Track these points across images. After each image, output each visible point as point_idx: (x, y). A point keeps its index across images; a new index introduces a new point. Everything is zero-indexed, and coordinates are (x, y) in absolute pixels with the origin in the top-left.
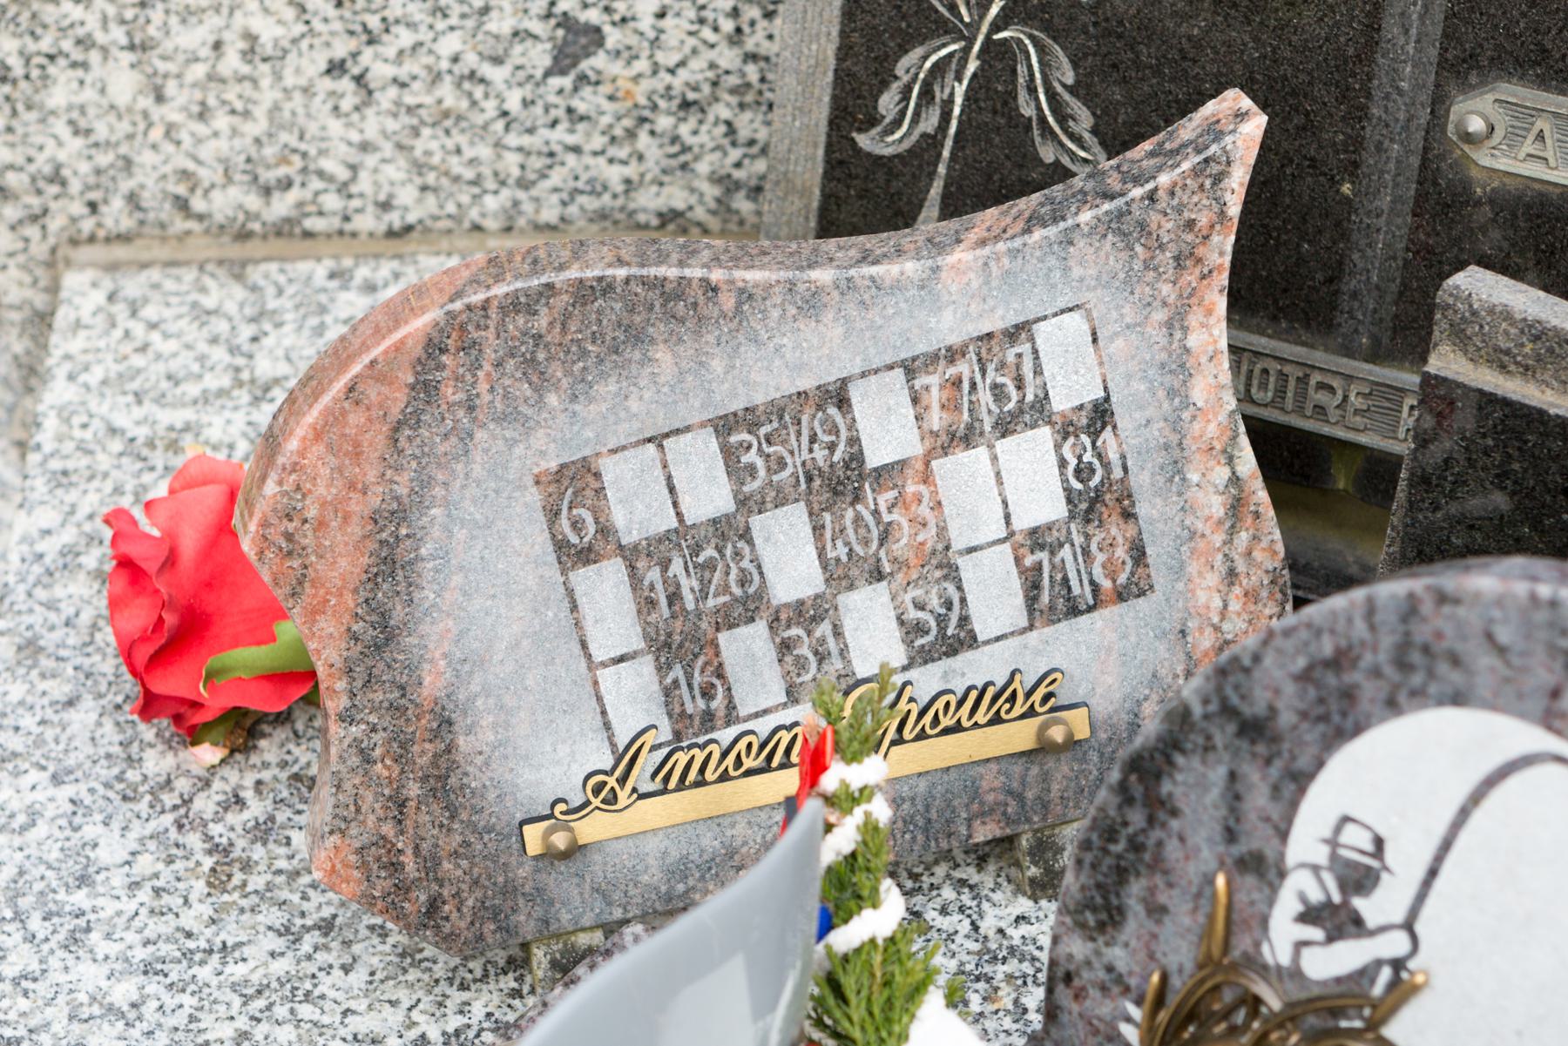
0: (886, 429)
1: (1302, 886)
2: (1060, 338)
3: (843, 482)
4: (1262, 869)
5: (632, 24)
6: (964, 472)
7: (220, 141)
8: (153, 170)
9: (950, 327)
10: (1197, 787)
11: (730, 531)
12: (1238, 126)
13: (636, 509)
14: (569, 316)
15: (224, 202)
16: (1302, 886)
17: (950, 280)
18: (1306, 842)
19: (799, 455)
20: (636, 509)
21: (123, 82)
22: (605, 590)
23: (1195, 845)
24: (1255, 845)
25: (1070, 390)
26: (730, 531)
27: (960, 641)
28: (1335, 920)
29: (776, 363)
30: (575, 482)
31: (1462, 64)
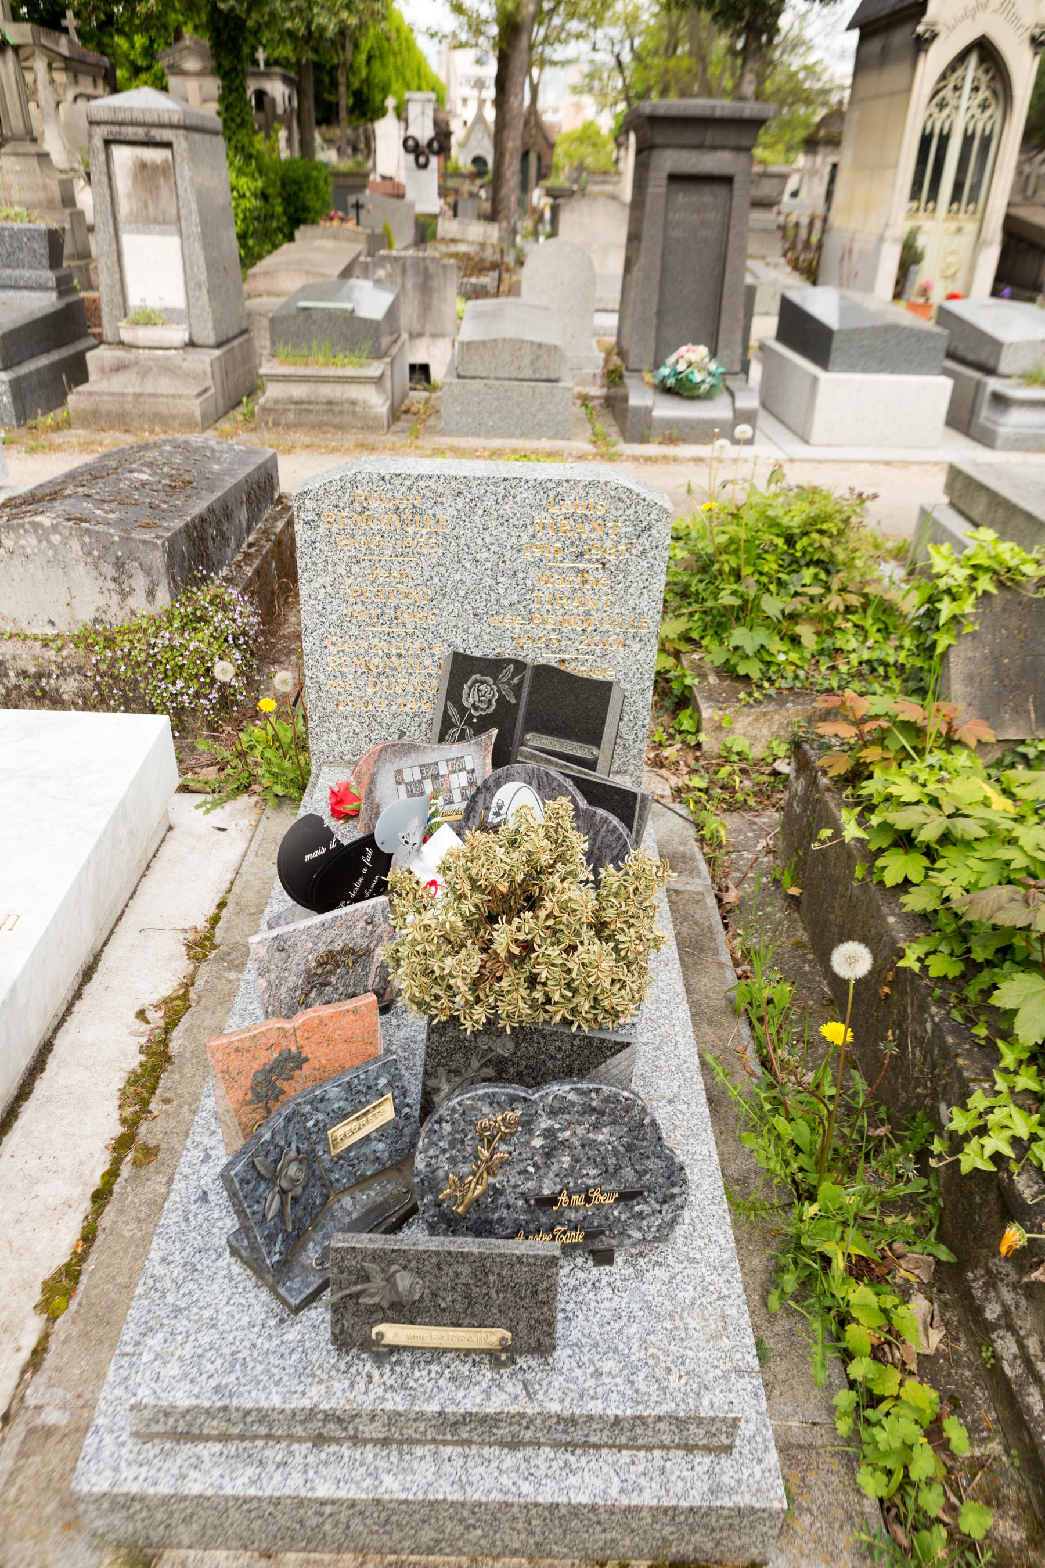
0: (443, 770)
1: (493, 810)
2: (468, 758)
3: (436, 777)
4: (488, 808)
5: (450, 213)
6: (453, 776)
7: (348, 747)
8: (337, 751)
9: (453, 755)
10: (480, 799)
11: (420, 782)
12: (495, 732)
13: (408, 778)
14: (403, 748)
15: (348, 757)
16: (493, 810)
17: (453, 750)
18: (494, 804)
19: (431, 772)
20: (408, 778)
21: (334, 737)
22: (402, 788)
23: (480, 807)
24: (344, 123)
25: (469, 767)
26: (420, 782)
27: (451, 802)
28: (497, 814)
29: (428, 758)
30: (399, 772)
31: (526, 731)
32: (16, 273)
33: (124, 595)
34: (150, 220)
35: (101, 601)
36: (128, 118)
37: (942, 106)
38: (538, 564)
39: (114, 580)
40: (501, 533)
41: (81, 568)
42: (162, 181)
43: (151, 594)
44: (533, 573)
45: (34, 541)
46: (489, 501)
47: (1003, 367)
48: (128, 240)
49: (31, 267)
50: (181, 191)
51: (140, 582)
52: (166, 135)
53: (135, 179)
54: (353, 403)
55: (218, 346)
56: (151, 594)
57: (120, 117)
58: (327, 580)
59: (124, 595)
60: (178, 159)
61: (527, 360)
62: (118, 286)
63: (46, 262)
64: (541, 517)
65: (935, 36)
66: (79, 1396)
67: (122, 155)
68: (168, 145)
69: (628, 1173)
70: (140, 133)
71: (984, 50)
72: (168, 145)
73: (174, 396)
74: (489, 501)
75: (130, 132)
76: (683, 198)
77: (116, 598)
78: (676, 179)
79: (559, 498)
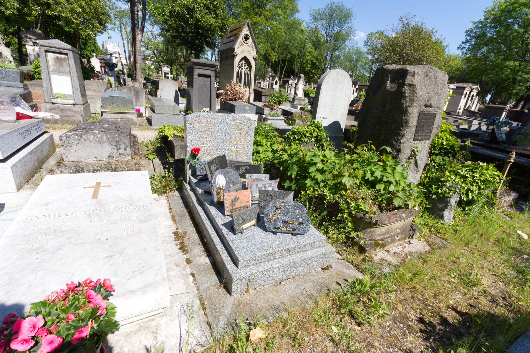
32: (7, 82)
33: (118, 150)
34: (58, 72)
35: (111, 151)
36: (53, 46)
37: (240, 68)
38: (233, 132)
39: (115, 146)
40: (226, 126)
41: (106, 143)
42: (64, 62)
43: (125, 149)
44: (232, 133)
45: (92, 137)
46: (224, 120)
47: (265, 113)
48: (53, 77)
49: (13, 81)
50: (71, 65)
51: (122, 146)
52: (66, 51)
53: (55, 61)
54: (128, 119)
55: (83, 105)
56: (125, 149)
57: (50, 45)
58: (193, 136)
59: (118, 150)
60: (70, 58)
61: (172, 110)
62: (50, 88)
63: (19, 80)
64: (233, 123)
65: (237, 55)
66: (428, 93)
67: (49, 54)
68: (67, 54)
69: (301, 220)
70: (57, 50)
71: (245, 59)
72: (67, 54)
73: (74, 116)
74: (224, 120)
75: (54, 50)
76: (201, 78)
77: (116, 150)
78: (200, 75)
79: (237, 119)
